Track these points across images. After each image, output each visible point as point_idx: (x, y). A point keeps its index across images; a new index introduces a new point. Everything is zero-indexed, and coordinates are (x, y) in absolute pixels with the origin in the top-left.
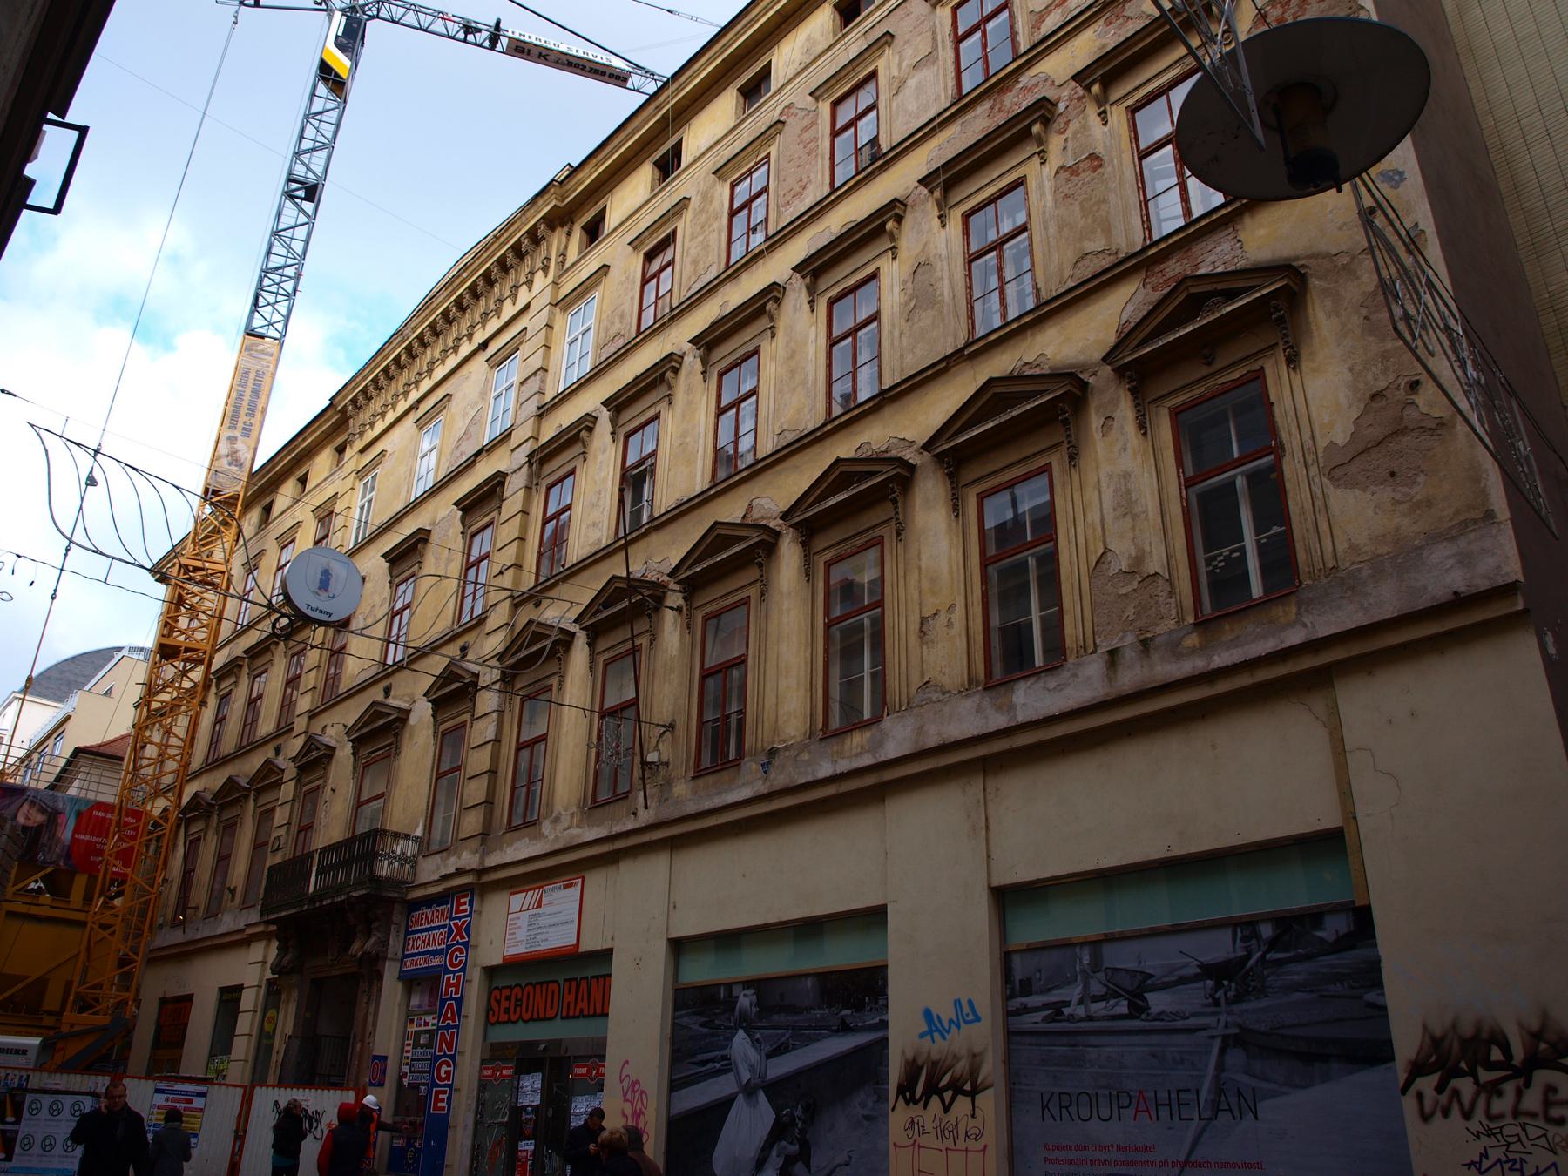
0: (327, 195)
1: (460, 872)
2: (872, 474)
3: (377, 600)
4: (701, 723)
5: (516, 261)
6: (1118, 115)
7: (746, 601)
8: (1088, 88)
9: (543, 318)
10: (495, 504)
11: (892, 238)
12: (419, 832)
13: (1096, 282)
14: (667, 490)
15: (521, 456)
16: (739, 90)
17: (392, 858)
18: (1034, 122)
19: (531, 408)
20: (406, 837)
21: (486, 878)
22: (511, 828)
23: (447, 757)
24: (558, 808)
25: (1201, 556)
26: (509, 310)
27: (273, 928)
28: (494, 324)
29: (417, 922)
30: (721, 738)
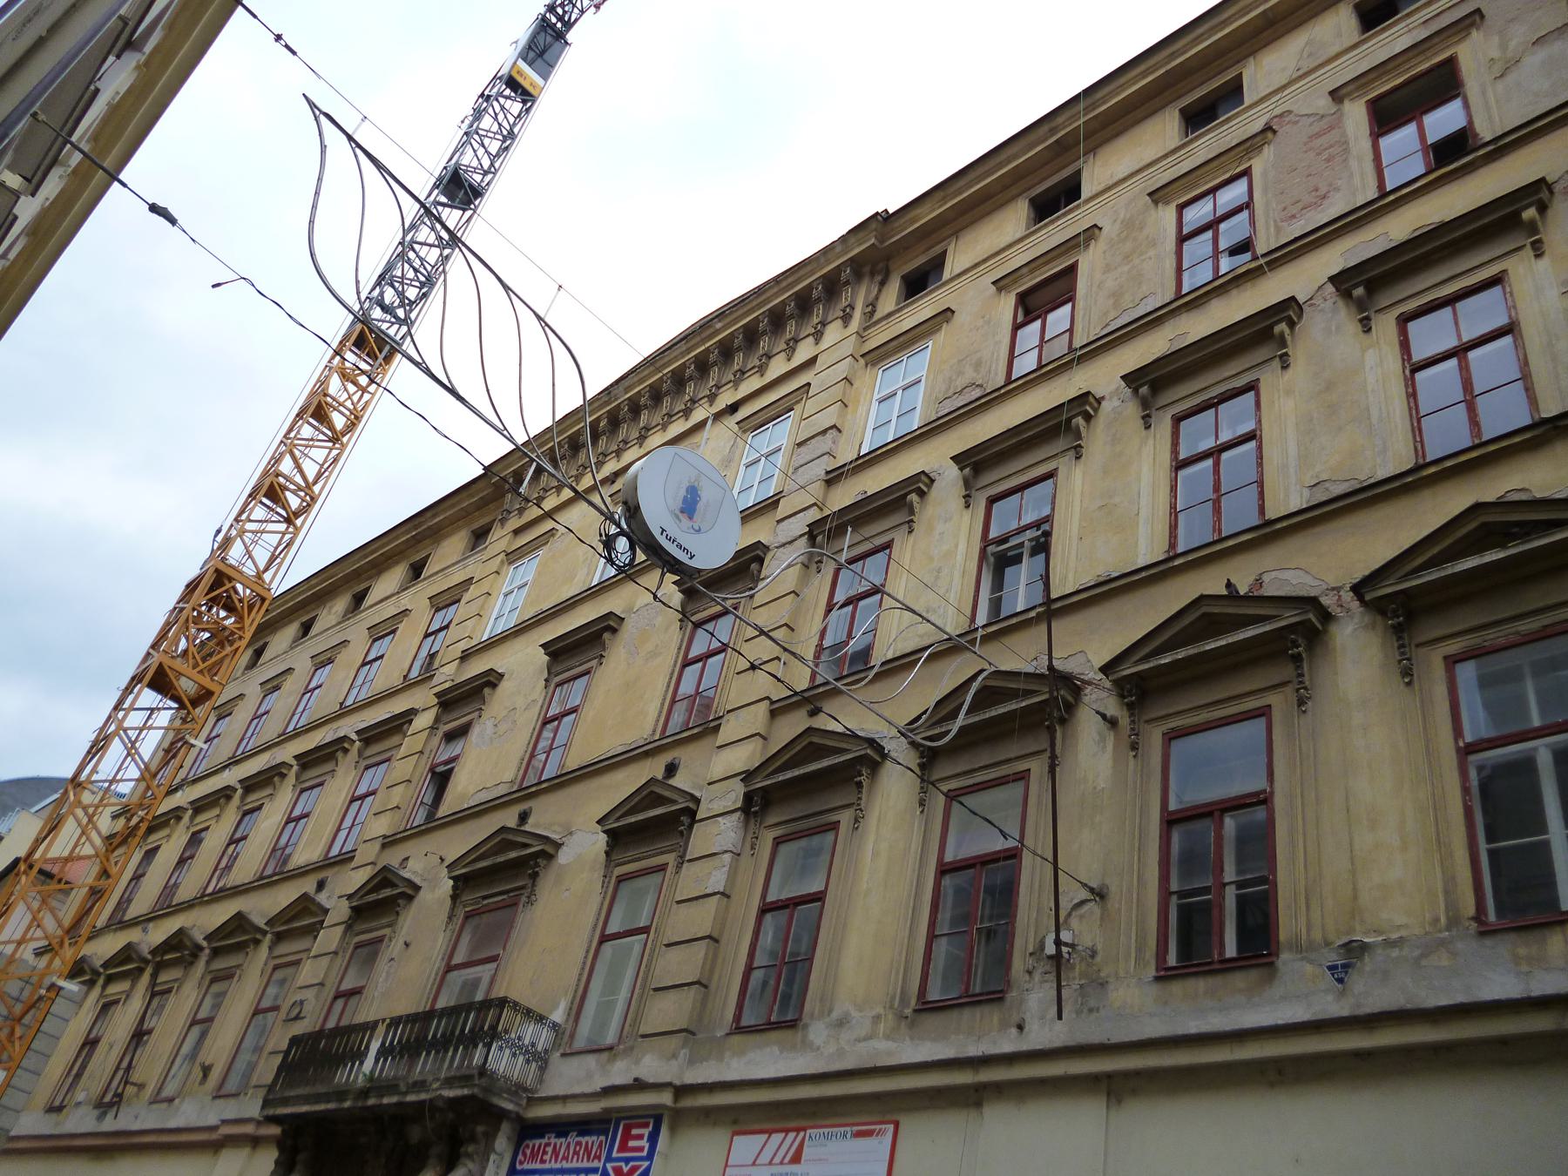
0: (248, 474)
1: (639, 1086)
2: (1028, 693)
3: (520, 702)
4: (1165, 893)
5: (629, 415)
6: (1386, 325)
7: (834, 826)
8: (1136, 391)
9: (842, 369)
10: (596, 652)
11: (1283, 343)
12: (558, 1016)
13: (1341, 504)
14: (465, 788)
15: (799, 525)
16: (1182, 111)
17: (518, 1048)
18: (1356, 286)
19: (819, 469)
20: (541, 1019)
21: (688, 1102)
22: (739, 1029)
23: (272, 991)
24: (842, 1006)
25: (1483, 846)
26: (778, 367)
27: (275, 1130)
28: (752, 384)
29: (533, 1156)
30: (1221, 912)
